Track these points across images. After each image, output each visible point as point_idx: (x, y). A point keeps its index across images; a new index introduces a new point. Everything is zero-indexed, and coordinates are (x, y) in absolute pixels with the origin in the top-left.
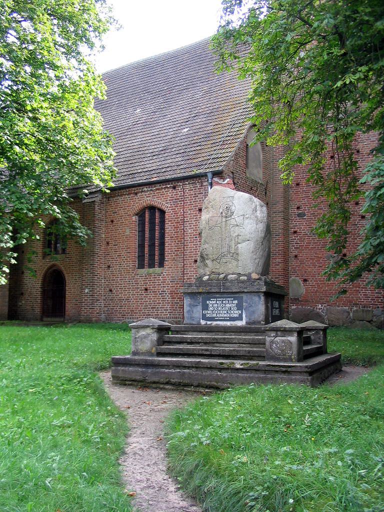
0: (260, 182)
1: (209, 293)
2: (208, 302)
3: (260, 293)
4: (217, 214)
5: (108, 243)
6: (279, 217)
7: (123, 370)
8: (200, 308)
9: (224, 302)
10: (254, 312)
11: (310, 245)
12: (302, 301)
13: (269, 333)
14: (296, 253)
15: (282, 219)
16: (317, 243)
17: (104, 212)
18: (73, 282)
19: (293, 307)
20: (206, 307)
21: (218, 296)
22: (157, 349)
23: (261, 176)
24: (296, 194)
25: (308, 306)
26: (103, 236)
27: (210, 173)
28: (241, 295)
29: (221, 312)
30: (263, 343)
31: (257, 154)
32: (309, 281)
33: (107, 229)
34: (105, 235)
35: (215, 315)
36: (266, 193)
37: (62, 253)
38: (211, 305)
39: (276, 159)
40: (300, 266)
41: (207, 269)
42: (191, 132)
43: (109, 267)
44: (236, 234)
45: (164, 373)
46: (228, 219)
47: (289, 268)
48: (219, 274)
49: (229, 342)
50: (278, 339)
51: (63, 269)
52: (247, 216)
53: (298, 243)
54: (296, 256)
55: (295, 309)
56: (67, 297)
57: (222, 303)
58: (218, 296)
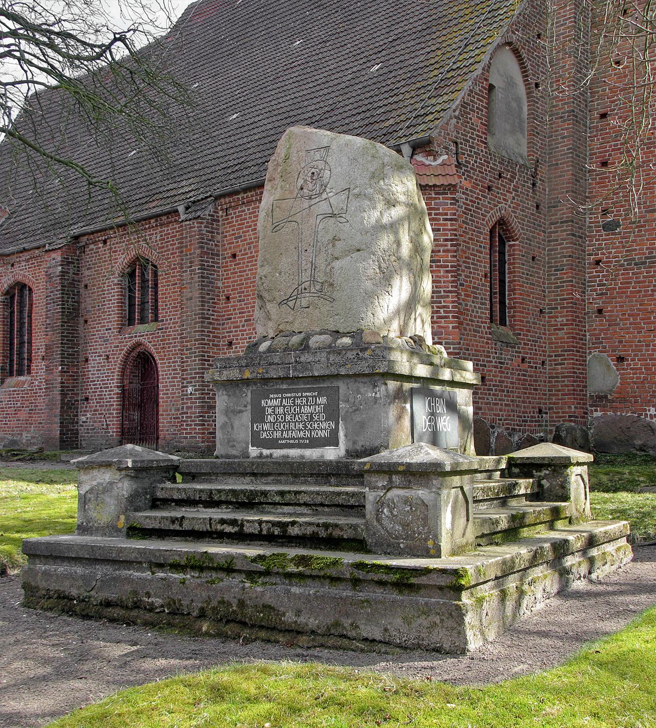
0: (521, 162)
1: (266, 381)
3: (377, 378)
4: (291, 192)
5: (228, 298)
6: (562, 231)
7: (45, 573)
8: (247, 417)
10: (362, 425)
11: (629, 288)
12: (613, 401)
13: (373, 478)
14: (599, 304)
15: (568, 235)
16: (645, 282)
18: (170, 374)
19: (595, 414)
20: (259, 415)
21: (285, 387)
22: (127, 519)
23: (524, 150)
24: (599, 183)
25: (627, 412)
27: (407, 145)
28: (335, 384)
29: (292, 426)
30: (356, 508)
31: (514, 105)
32: (627, 360)
33: (225, 271)
34: (223, 283)
35: (279, 434)
36: (534, 185)
37: (152, 321)
38: (270, 410)
39: (558, 114)
40: (607, 329)
41: (270, 324)
42: (385, 70)
44: (330, 237)
45: (128, 580)
46: (313, 202)
47: (585, 335)
49: (285, 500)
50: (395, 493)
52: (356, 191)
53: (604, 285)
54: (600, 311)
55: (601, 417)
56: (161, 404)
57: (294, 403)
58: (285, 387)
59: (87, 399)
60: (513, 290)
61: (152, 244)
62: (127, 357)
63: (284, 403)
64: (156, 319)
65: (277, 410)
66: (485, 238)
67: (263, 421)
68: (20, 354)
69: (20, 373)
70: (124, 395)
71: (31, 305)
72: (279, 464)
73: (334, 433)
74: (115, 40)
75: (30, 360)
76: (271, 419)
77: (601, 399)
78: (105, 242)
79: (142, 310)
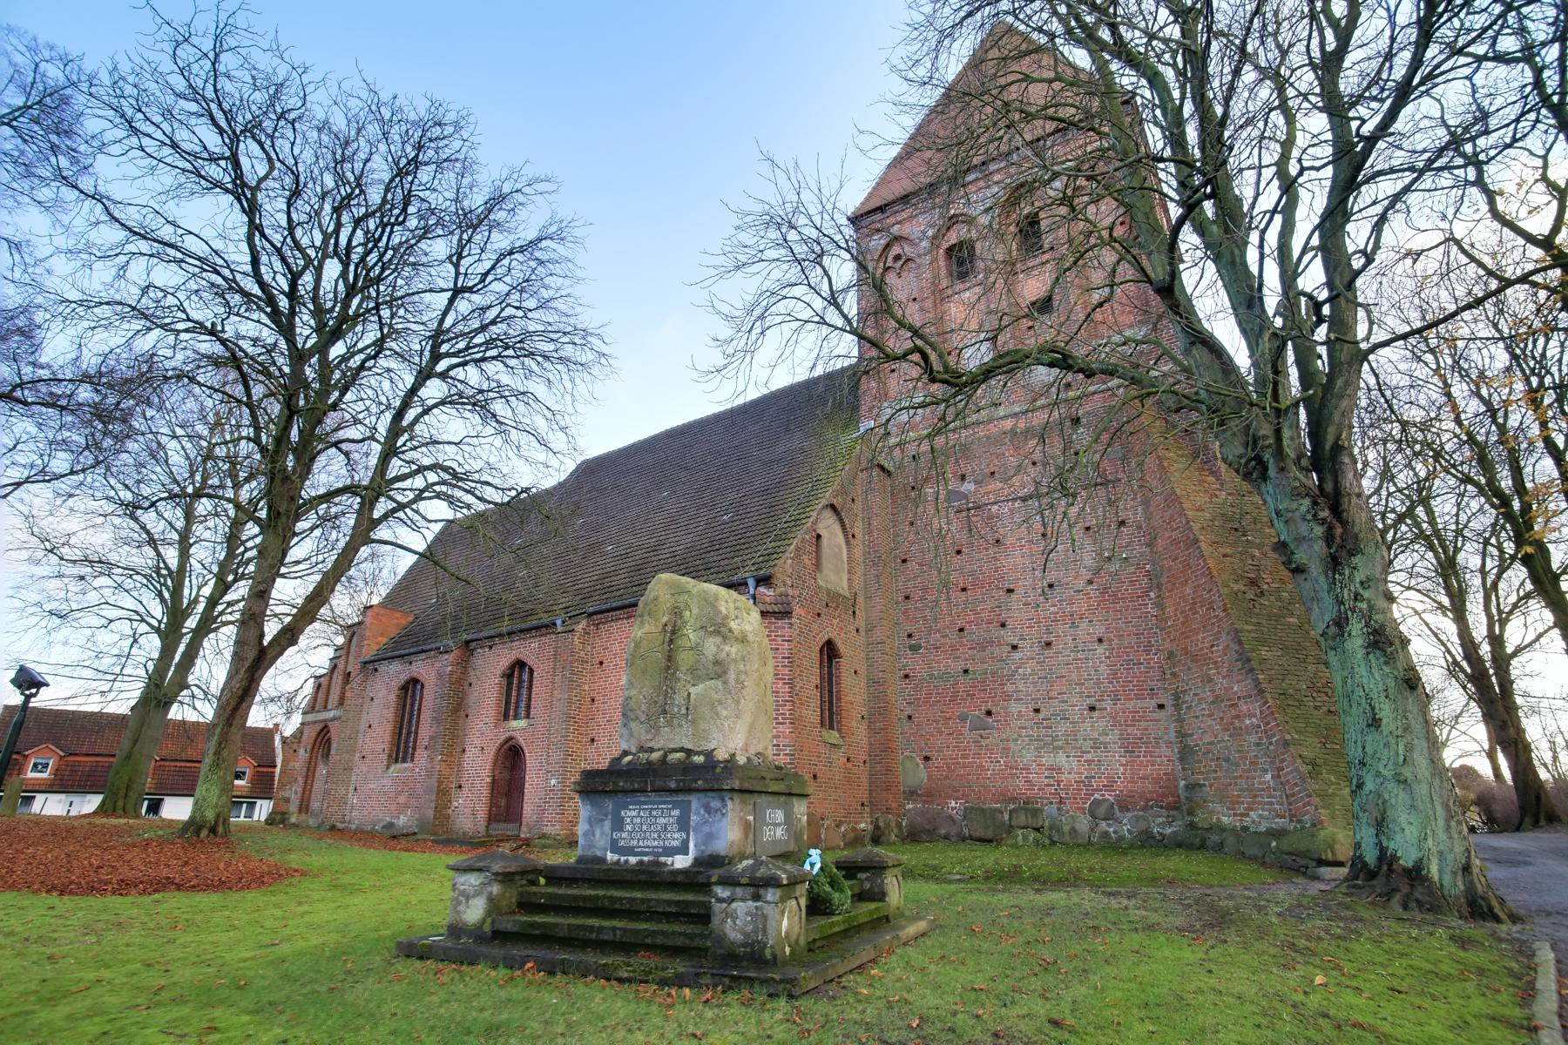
8: (607, 825)
14: (908, 711)
20: (618, 825)
22: (493, 922)
23: (845, 583)
48: (652, 750)
51: (522, 743)
60: (839, 699)
61: (530, 650)
62: (502, 745)
64: (528, 716)
66: (815, 656)
68: (407, 742)
69: (404, 760)
72: (633, 871)
73: (685, 843)
75: (414, 749)
76: (629, 828)
77: (912, 794)
79: (517, 707)
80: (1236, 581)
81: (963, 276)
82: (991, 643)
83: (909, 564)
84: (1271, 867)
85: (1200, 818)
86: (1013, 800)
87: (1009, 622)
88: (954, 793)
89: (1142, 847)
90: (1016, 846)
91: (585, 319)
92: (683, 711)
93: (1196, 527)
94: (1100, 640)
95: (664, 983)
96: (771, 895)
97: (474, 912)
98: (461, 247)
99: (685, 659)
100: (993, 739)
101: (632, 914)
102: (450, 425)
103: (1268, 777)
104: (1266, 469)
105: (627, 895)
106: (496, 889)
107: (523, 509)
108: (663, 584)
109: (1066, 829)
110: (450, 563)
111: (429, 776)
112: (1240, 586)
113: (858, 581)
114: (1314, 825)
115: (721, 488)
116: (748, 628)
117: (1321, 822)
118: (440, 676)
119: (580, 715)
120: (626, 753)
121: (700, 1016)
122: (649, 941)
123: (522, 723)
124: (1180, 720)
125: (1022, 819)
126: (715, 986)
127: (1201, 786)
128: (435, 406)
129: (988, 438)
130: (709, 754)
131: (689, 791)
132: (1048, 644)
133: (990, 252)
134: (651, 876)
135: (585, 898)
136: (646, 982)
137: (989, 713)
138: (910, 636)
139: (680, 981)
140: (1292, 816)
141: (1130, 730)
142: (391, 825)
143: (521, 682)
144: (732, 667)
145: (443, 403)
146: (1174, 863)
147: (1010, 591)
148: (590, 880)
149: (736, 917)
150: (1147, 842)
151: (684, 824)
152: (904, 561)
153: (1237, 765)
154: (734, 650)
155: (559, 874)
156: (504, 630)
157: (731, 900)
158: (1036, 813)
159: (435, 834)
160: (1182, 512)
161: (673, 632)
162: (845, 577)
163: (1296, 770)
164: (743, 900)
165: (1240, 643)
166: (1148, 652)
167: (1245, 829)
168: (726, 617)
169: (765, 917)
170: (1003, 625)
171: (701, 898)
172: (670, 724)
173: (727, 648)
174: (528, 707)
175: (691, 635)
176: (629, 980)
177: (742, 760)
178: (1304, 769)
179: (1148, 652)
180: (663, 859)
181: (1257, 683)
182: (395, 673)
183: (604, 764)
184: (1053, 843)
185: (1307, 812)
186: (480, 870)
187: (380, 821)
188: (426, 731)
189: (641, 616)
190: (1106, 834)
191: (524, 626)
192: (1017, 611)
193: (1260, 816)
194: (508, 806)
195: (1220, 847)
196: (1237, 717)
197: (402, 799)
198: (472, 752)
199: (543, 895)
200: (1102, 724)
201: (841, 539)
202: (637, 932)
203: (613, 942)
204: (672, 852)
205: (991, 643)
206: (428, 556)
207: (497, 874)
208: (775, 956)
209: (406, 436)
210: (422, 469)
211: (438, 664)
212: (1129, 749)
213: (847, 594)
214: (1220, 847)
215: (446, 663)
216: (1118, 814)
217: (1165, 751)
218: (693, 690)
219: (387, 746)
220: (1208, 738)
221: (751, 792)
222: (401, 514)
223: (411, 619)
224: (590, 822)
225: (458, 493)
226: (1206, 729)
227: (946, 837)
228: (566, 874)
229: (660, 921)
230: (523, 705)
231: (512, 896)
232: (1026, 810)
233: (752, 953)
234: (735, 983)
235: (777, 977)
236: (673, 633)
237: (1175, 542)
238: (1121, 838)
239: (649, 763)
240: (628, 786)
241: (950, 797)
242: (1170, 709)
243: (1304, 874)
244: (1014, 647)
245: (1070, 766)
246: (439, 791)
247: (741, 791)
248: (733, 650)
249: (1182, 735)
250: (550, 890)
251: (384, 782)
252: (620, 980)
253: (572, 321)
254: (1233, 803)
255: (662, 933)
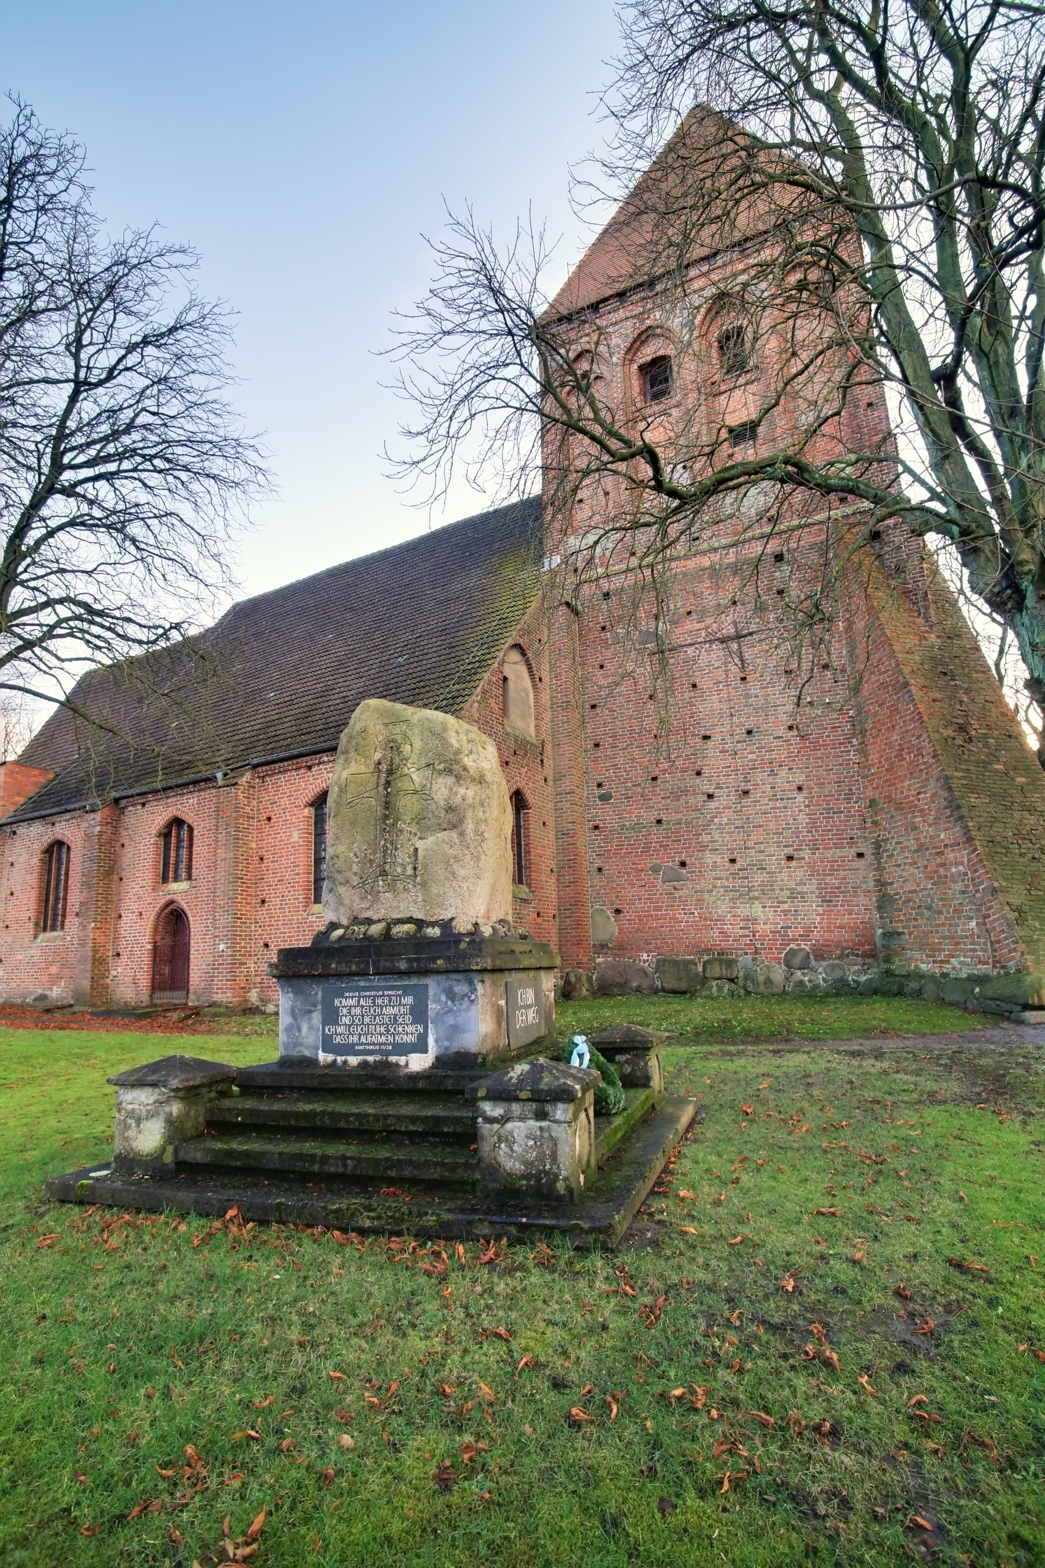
2: (337, 1002)
5: (262, 859)
8: (317, 1018)
9: (379, 1001)
10: (455, 1029)
14: (598, 863)
17: (255, 803)
20: (331, 1017)
21: (362, 984)
23: (532, 731)
26: (254, 845)
35: (356, 1039)
38: (345, 1011)
41: (342, 910)
43: (263, 902)
48: (369, 922)
51: (185, 907)
54: (600, 870)
59: (118, 955)
60: (528, 852)
61: (188, 806)
63: (362, 1002)
64: (189, 878)
65: (353, 1011)
67: (336, 1023)
68: (55, 909)
69: (54, 928)
70: (155, 950)
71: (68, 862)
72: (358, 1077)
74: (172, 628)
75: (64, 916)
76: (346, 1020)
77: (602, 947)
78: (144, 804)
80: (946, 727)
81: (656, 396)
82: (685, 792)
83: (598, 710)
84: (974, 1012)
85: (897, 965)
86: (707, 951)
87: (705, 770)
88: (646, 945)
89: (838, 995)
90: (710, 997)
91: (234, 429)
92: (410, 871)
93: (906, 670)
94: (800, 789)
95: (424, 1235)
96: (561, 1111)
97: (149, 1138)
98: (80, 332)
99: (408, 806)
100: (687, 890)
101: (363, 1134)
102: (84, 549)
103: (973, 924)
104: (1023, 598)
105: (354, 1110)
106: (176, 1108)
107: (175, 663)
108: (371, 715)
109: (761, 979)
110: (93, 711)
111: (83, 944)
112: (949, 732)
113: (546, 726)
114: (1019, 971)
115: (416, 615)
116: (485, 765)
117: (1026, 968)
118: (88, 837)
119: (248, 880)
120: (333, 926)
121: (489, 1291)
122: (393, 1173)
123: (183, 885)
124: (880, 869)
125: (716, 970)
126: (498, 1239)
127: (900, 934)
128: (61, 528)
129: (685, 574)
130: (446, 925)
131: (426, 972)
132: (746, 793)
133: (686, 373)
134: (380, 1082)
135: (297, 1115)
136: (399, 1234)
137: (683, 864)
138: (600, 785)
139: (447, 1233)
140: (995, 962)
141: (828, 879)
142: (43, 997)
143: (179, 841)
144: (469, 814)
145: (72, 523)
146: (878, 1012)
147: (706, 738)
148: (299, 1089)
149: (513, 1140)
150: (841, 989)
151: (419, 1014)
152: (593, 707)
153: (940, 912)
154: (470, 793)
155: (259, 1082)
156: (159, 786)
157: (504, 1120)
158: (730, 963)
159: (94, 1005)
160: (892, 655)
161: (390, 772)
162: (532, 723)
163: (1004, 917)
164: (522, 1119)
165: (950, 789)
166: (848, 800)
167: (945, 975)
168: (458, 752)
169: (554, 1141)
170: (699, 773)
171: (465, 1113)
172: (392, 888)
173: (462, 791)
174: (189, 868)
175: (414, 775)
176: (376, 1232)
177: (487, 931)
178: (1012, 916)
179: (848, 800)
180: (393, 1059)
181: (967, 830)
182: (34, 837)
183: (305, 941)
184: (748, 993)
185: (1013, 958)
186: (154, 1085)
187: (31, 993)
188: (75, 897)
189: (346, 752)
190: (801, 982)
191: (180, 781)
192: (713, 760)
193: (962, 963)
194: (173, 973)
195: (918, 993)
196: (943, 865)
197: (54, 970)
198: (128, 918)
199: (241, 1112)
200: (800, 874)
201: (527, 683)
202: (376, 1162)
203: (342, 1176)
204: (405, 1049)
205: (685, 792)
206: (70, 705)
207: (177, 1090)
208: (570, 1190)
209: (28, 560)
210: (49, 603)
211: (84, 825)
212: (827, 899)
213: (535, 742)
214: (918, 993)
215: (94, 822)
216: (813, 963)
217: (863, 900)
218: (419, 844)
219: (32, 914)
220: (909, 886)
221: (501, 970)
222: (27, 654)
223: (51, 776)
224: (293, 1013)
225: (95, 630)
226: (907, 877)
227: (638, 990)
228: (268, 1081)
229: (400, 1145)
230: (183, 866)
231: (199, 1114)
232: (721, 961)
233: (539, 1187)
234: (523, 1237)
235: (586, 1226)
236: (389, 774)
237: (884, 686)
238: (818, 986)
239: (367, 938)
240: (343, 968)
241: (641, 950)
242: (869, 858)
243: (1009, 1019)
244: (710, 796)
245: (765, 917)
246: (94, 960)
247: (493, 971)
248: (468, 792)
249: (881, 883)
250: (249, 1104)
251: (33, 952)
252: (363, 1232)
253: (221, 432)
254: (933, 950)
255: (411, 1163)
